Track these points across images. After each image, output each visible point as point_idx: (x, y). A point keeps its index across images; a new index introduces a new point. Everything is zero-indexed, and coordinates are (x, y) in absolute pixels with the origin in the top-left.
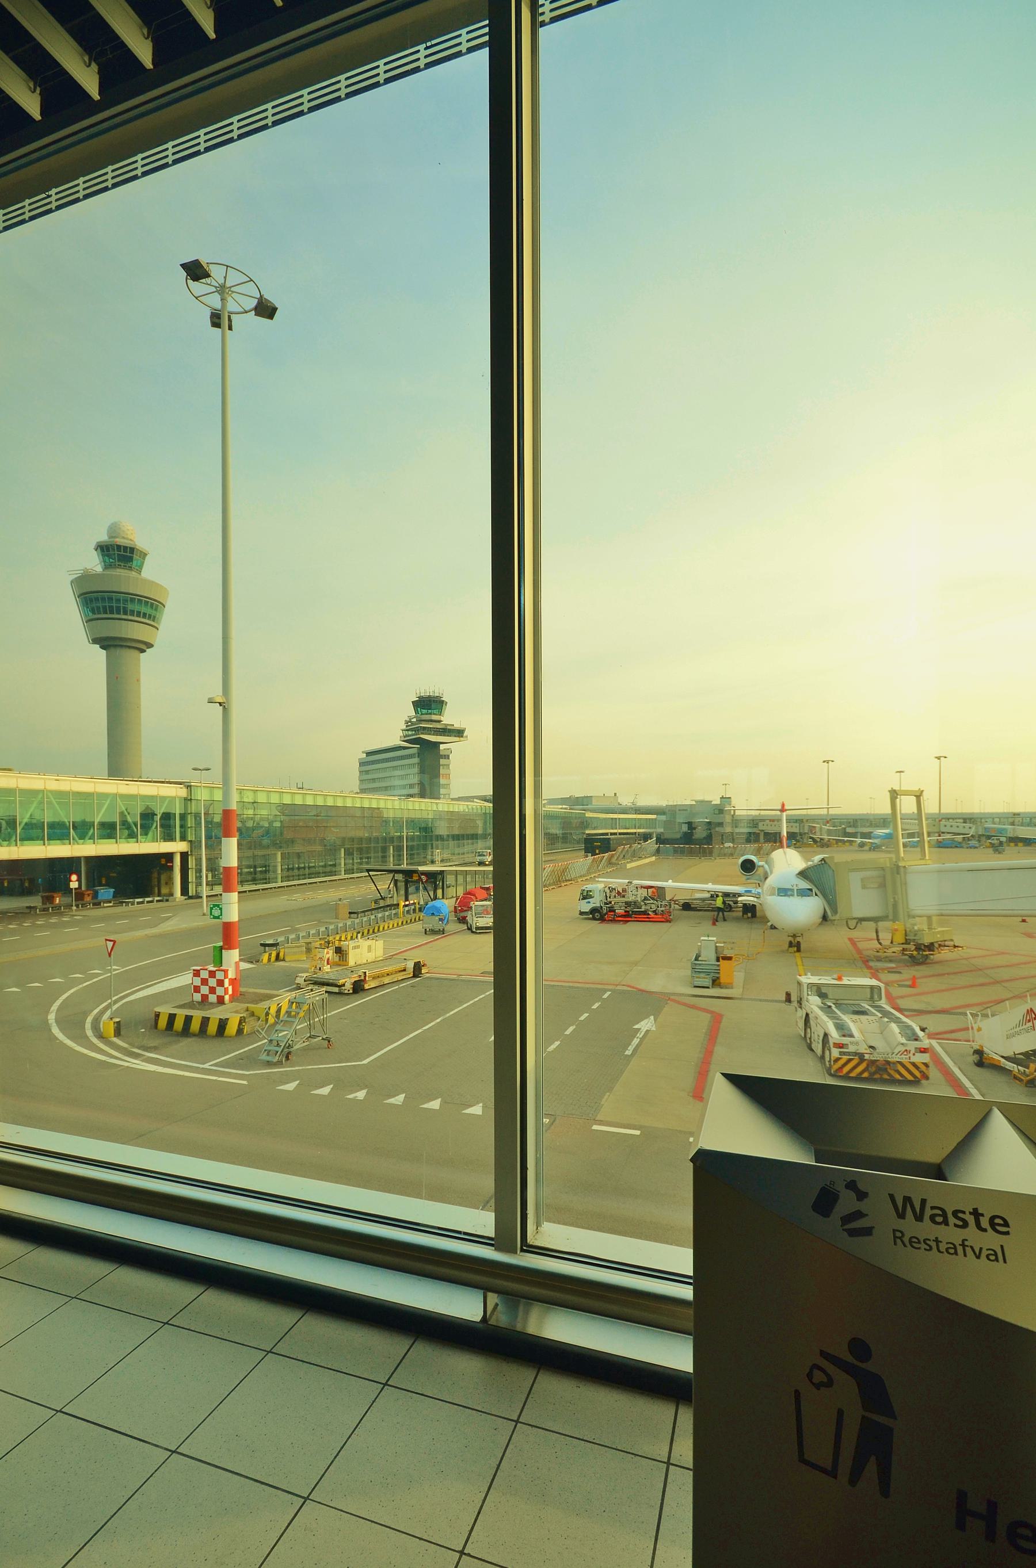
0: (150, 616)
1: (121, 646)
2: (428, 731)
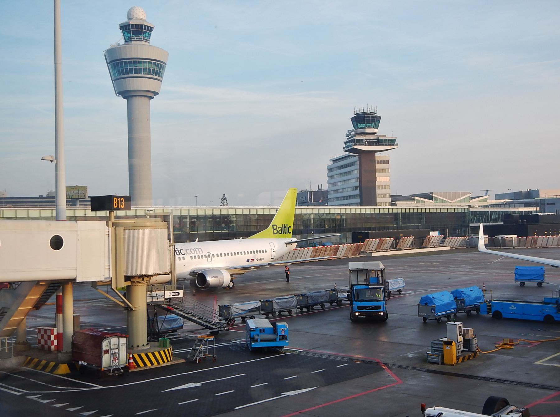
1: (136, 96)
2: (358, 142)
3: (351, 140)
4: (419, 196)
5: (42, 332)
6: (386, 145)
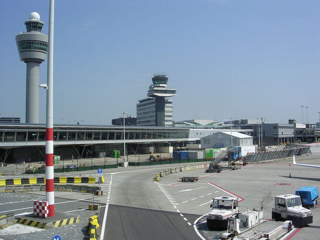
0: (44, 49)
3: (151, 91)
4: (187, 121)
5: (38, 204)
6: (171, 93)
